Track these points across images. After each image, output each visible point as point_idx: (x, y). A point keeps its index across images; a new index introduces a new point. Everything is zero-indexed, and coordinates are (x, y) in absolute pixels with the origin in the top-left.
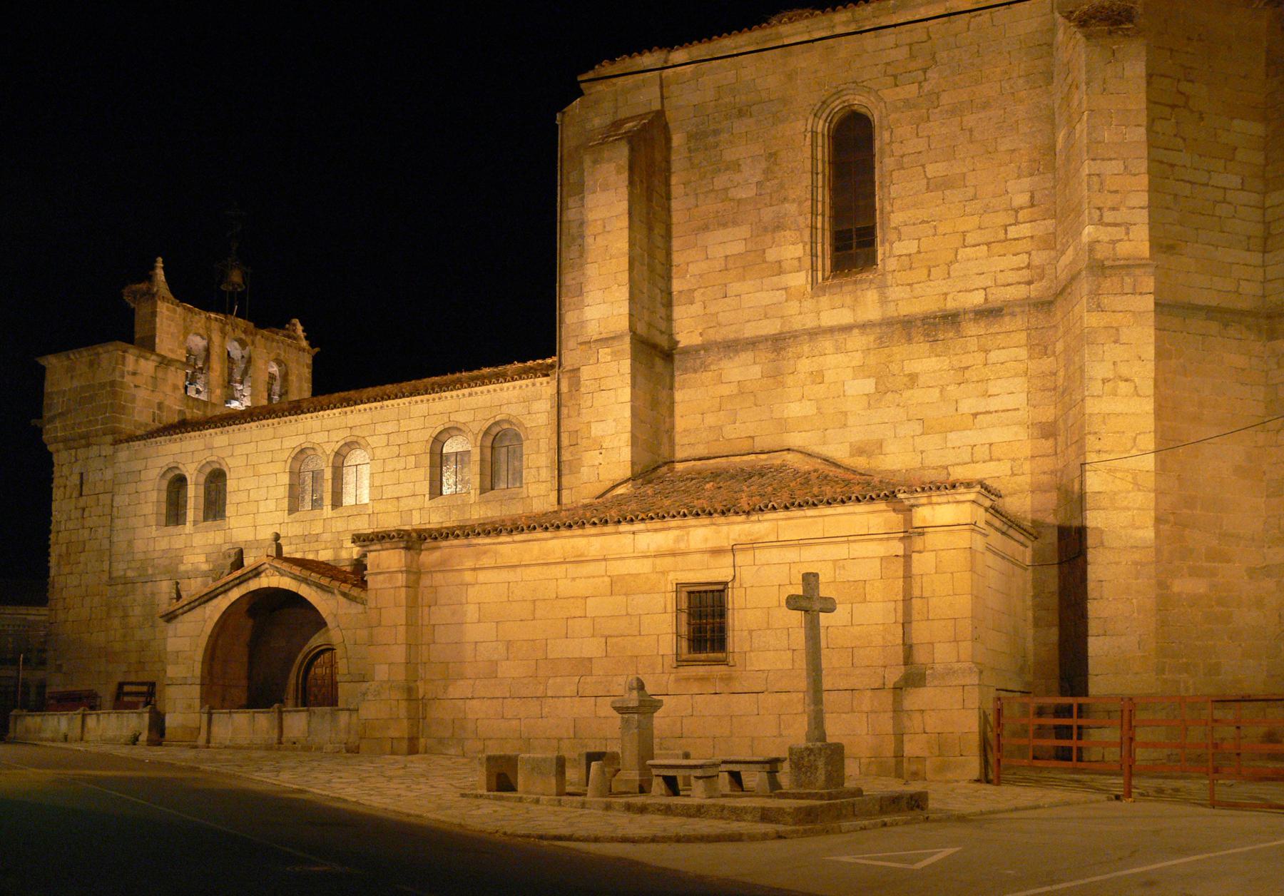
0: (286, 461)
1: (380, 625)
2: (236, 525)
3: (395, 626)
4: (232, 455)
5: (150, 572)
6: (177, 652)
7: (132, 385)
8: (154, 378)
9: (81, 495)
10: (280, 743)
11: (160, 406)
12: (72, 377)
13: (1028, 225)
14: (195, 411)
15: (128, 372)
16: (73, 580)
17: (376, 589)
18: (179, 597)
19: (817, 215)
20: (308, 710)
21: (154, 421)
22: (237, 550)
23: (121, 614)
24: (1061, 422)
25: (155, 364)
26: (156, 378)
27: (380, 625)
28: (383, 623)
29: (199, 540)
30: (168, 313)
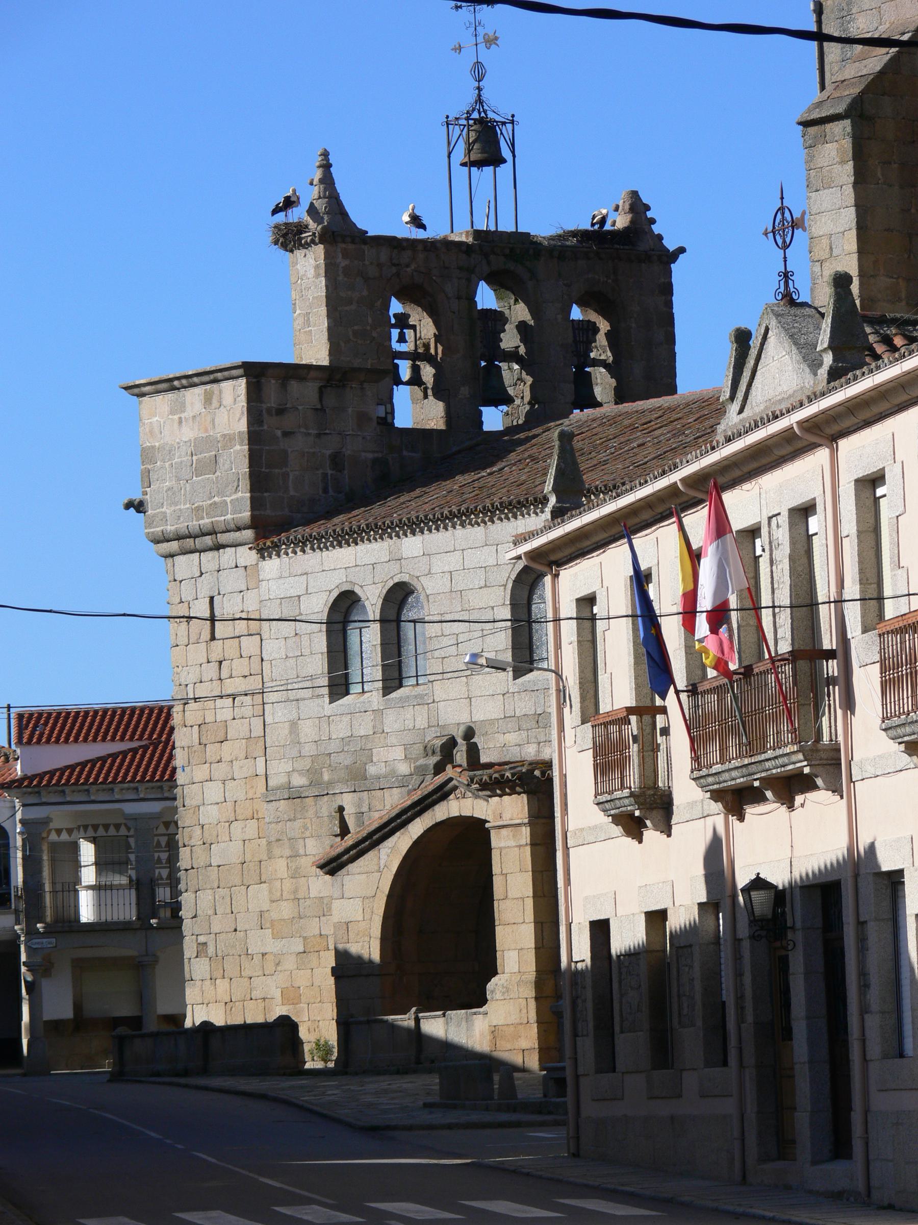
0: (505, 586)
1: (506, 898)
2: (444, 697)
3: (523, 899)
4: (429, 573)
5: (326, 777)
6: (347, 924)
7: (279, 433)
8: (320, 411)
9: (213, 638)
10: (418, 1062)
11: (336, 460)
12: (180, 421)
13: (399, 790)
14: (405, 453)
15: (269, 411)
16: (213, 792)
17: (501, 849)
18: (344, 831)
19: (557, 620)
20: (444, 1015)
21: (325, 491)
22: (444, 739)
23: (287, 852)
24: (612, 812)
25: (317, 384)
26: (323, 410)
27: (506, 898)
28: (510, 895)
29: (392, 721)
30: (346, 262)
